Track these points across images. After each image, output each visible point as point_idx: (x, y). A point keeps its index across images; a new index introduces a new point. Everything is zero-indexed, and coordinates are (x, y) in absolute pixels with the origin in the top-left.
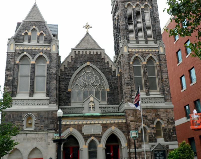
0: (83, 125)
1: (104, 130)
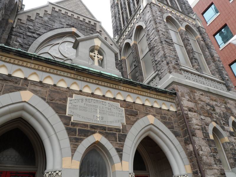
0: (69, 92)
1: (130, 123)
